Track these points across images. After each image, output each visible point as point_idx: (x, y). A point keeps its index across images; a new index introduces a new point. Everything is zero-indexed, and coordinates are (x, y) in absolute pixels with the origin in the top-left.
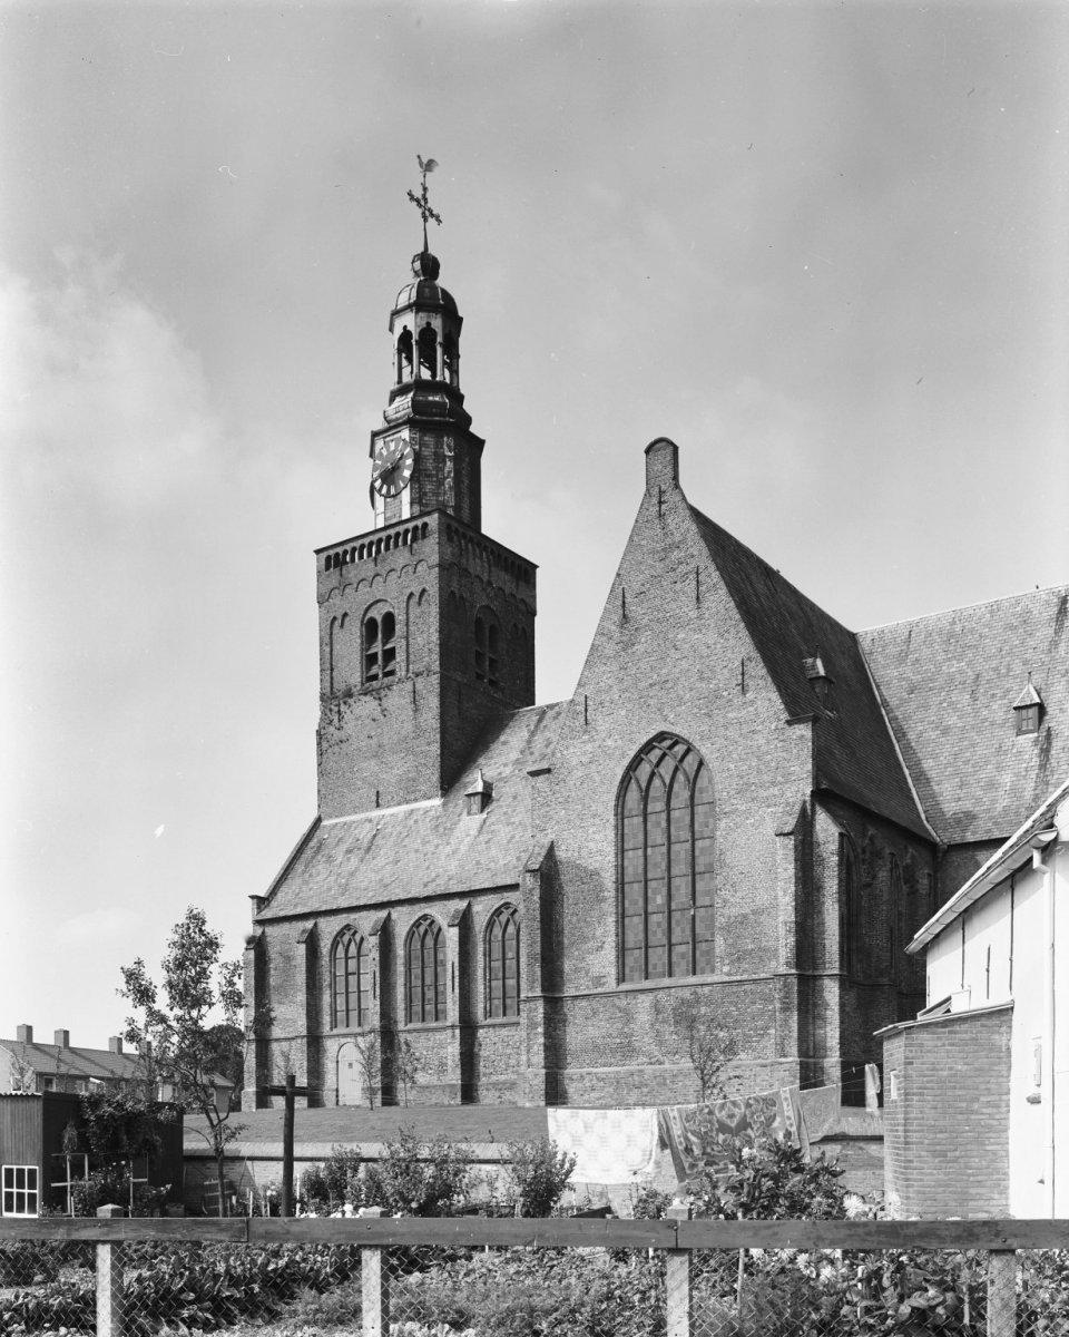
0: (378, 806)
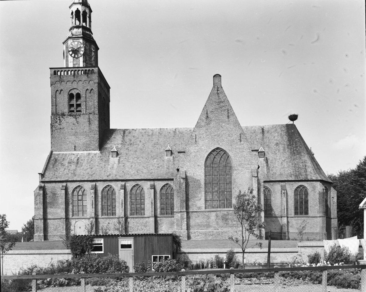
0: (75, 150)
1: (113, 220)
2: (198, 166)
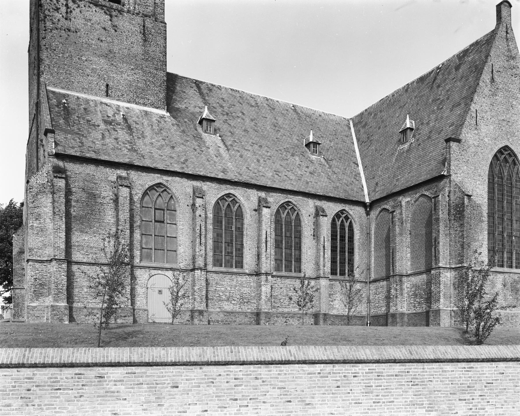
1: (239, 278)
2: (480, 175)
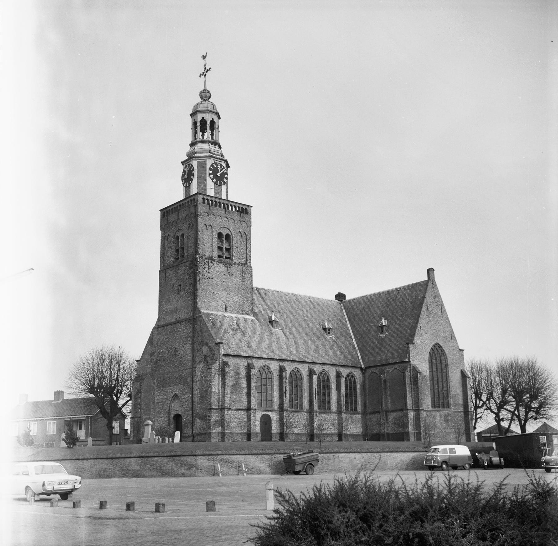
2: (424, 360)
